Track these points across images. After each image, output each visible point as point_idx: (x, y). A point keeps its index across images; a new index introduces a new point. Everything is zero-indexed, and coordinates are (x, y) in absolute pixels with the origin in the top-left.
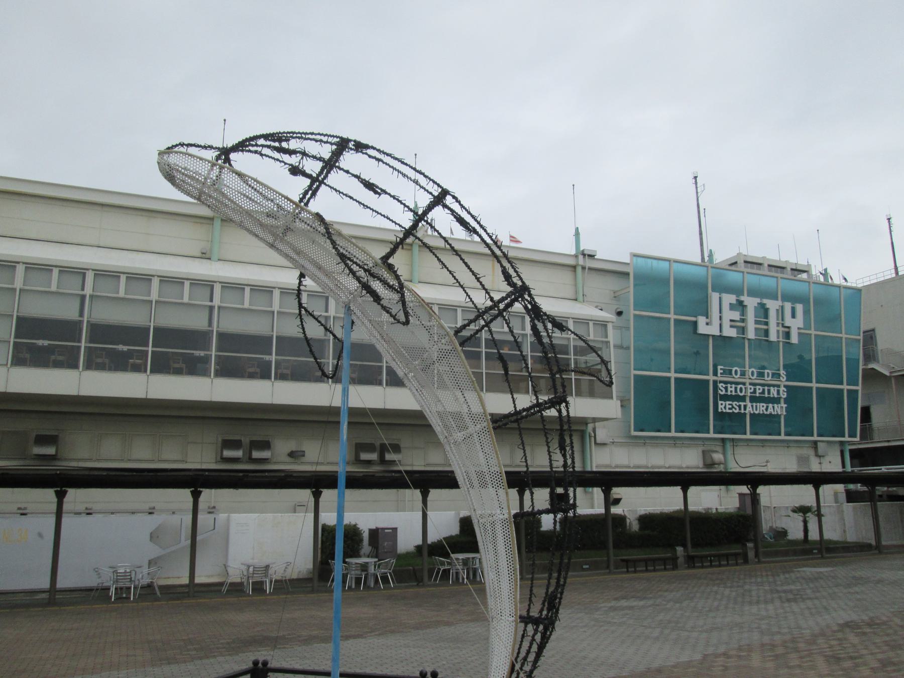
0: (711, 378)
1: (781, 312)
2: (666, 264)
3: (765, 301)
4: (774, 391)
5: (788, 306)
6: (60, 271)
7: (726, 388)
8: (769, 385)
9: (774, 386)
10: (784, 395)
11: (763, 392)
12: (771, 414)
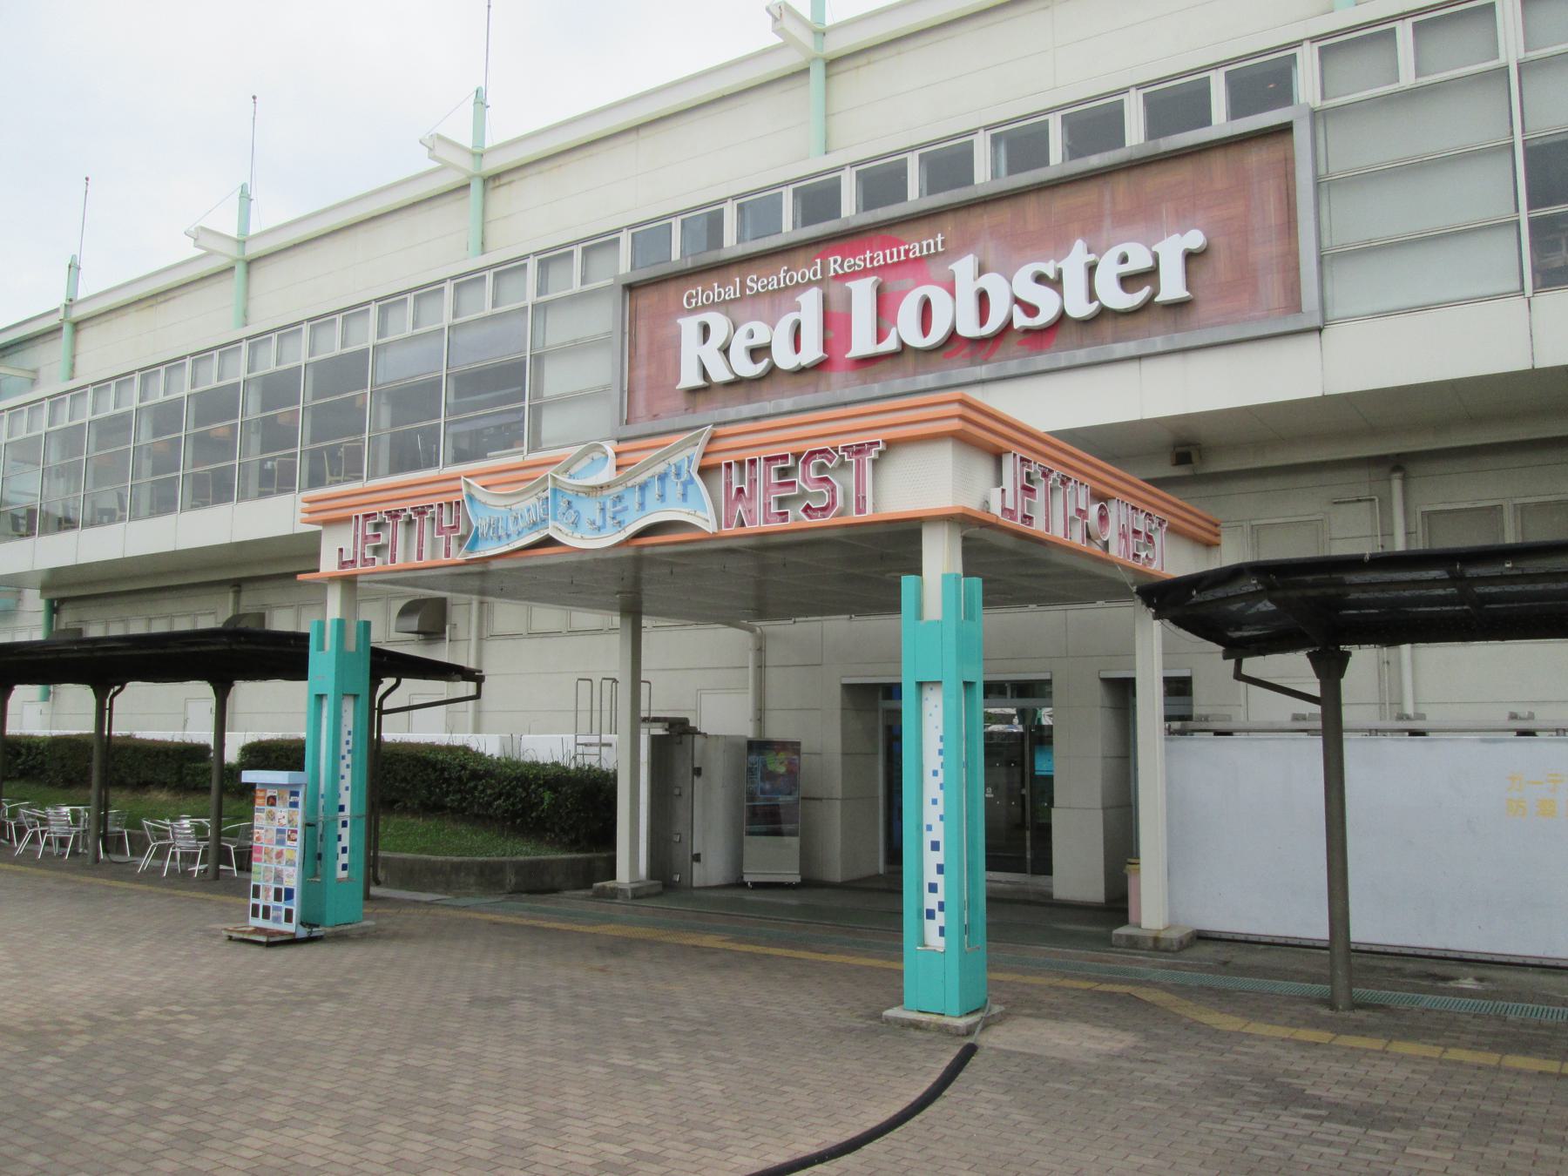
6: (1323, 51)
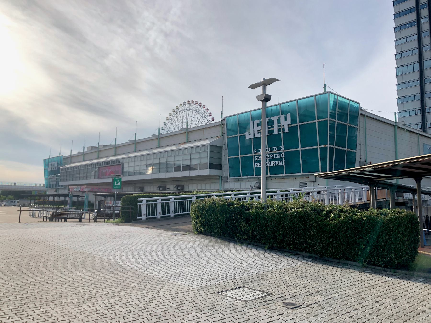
0: (253, 155)
1: (279, 122)
2: (313, 98)
3: (271, 118)
4: (278, 156)
5: (283, 117)
7: (258, 158)
8: (276, 153)
9: (278, 153)
10: (283, 157)
11: (273, 156)
12: (277, 165)
